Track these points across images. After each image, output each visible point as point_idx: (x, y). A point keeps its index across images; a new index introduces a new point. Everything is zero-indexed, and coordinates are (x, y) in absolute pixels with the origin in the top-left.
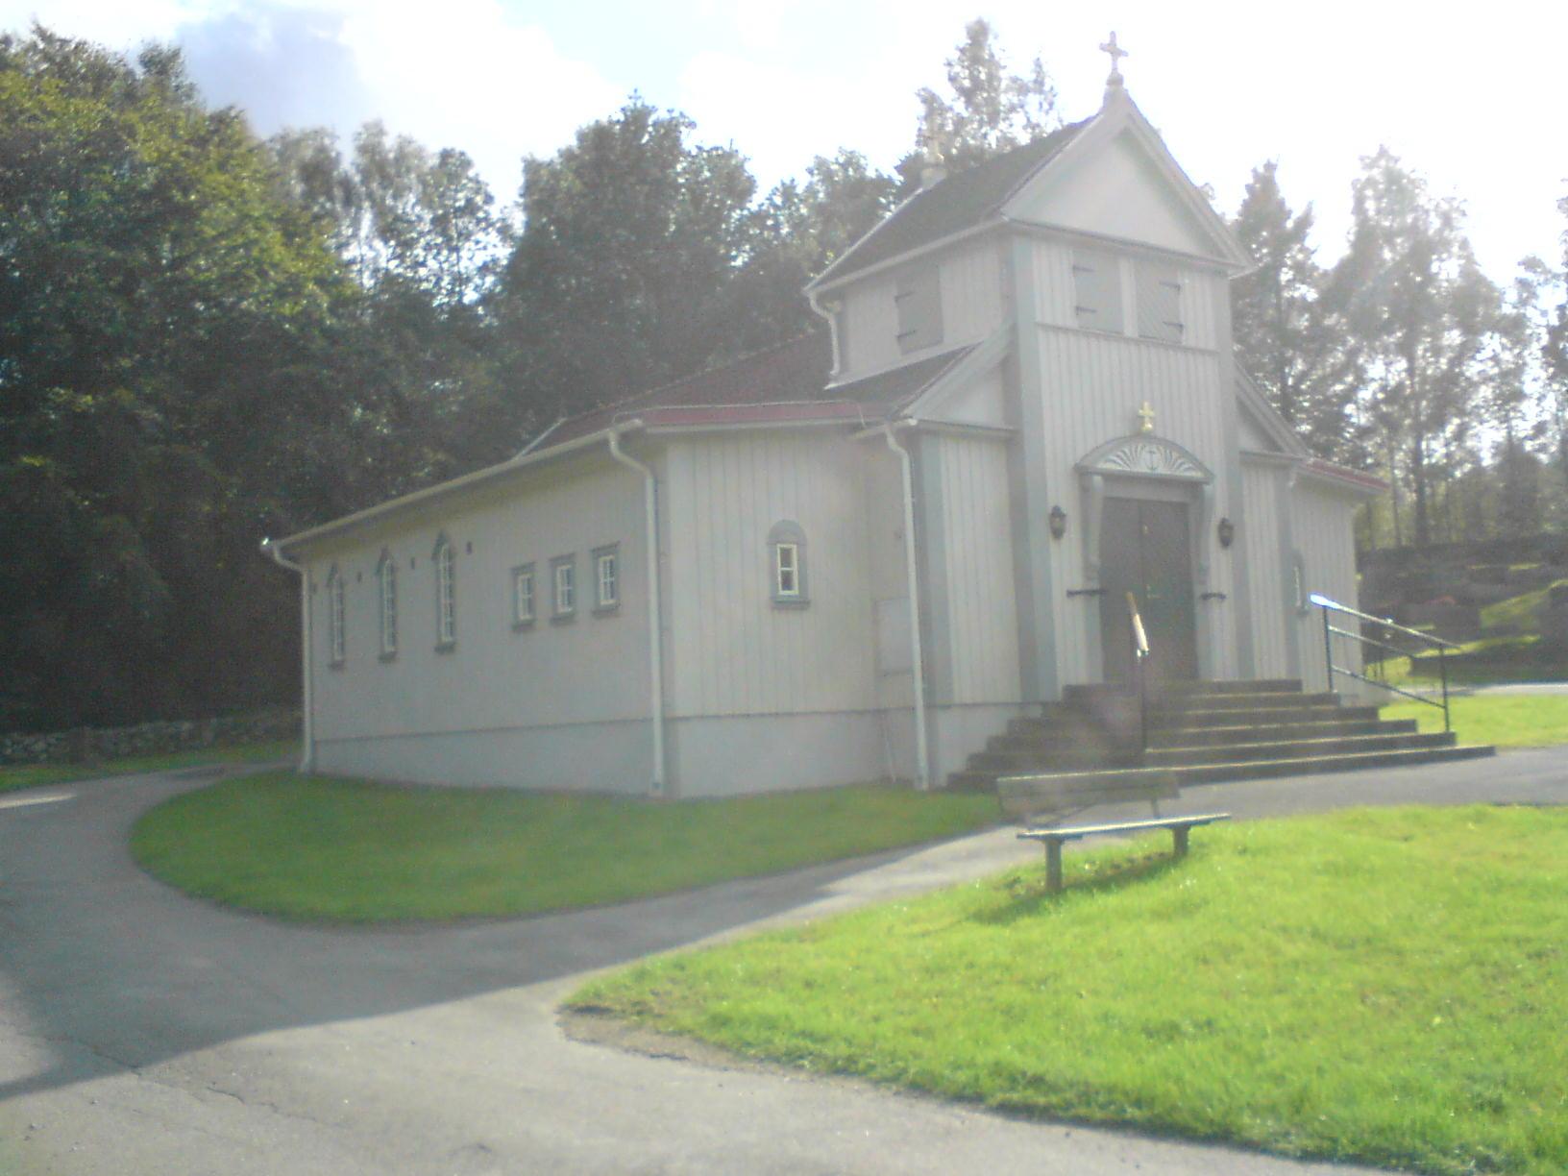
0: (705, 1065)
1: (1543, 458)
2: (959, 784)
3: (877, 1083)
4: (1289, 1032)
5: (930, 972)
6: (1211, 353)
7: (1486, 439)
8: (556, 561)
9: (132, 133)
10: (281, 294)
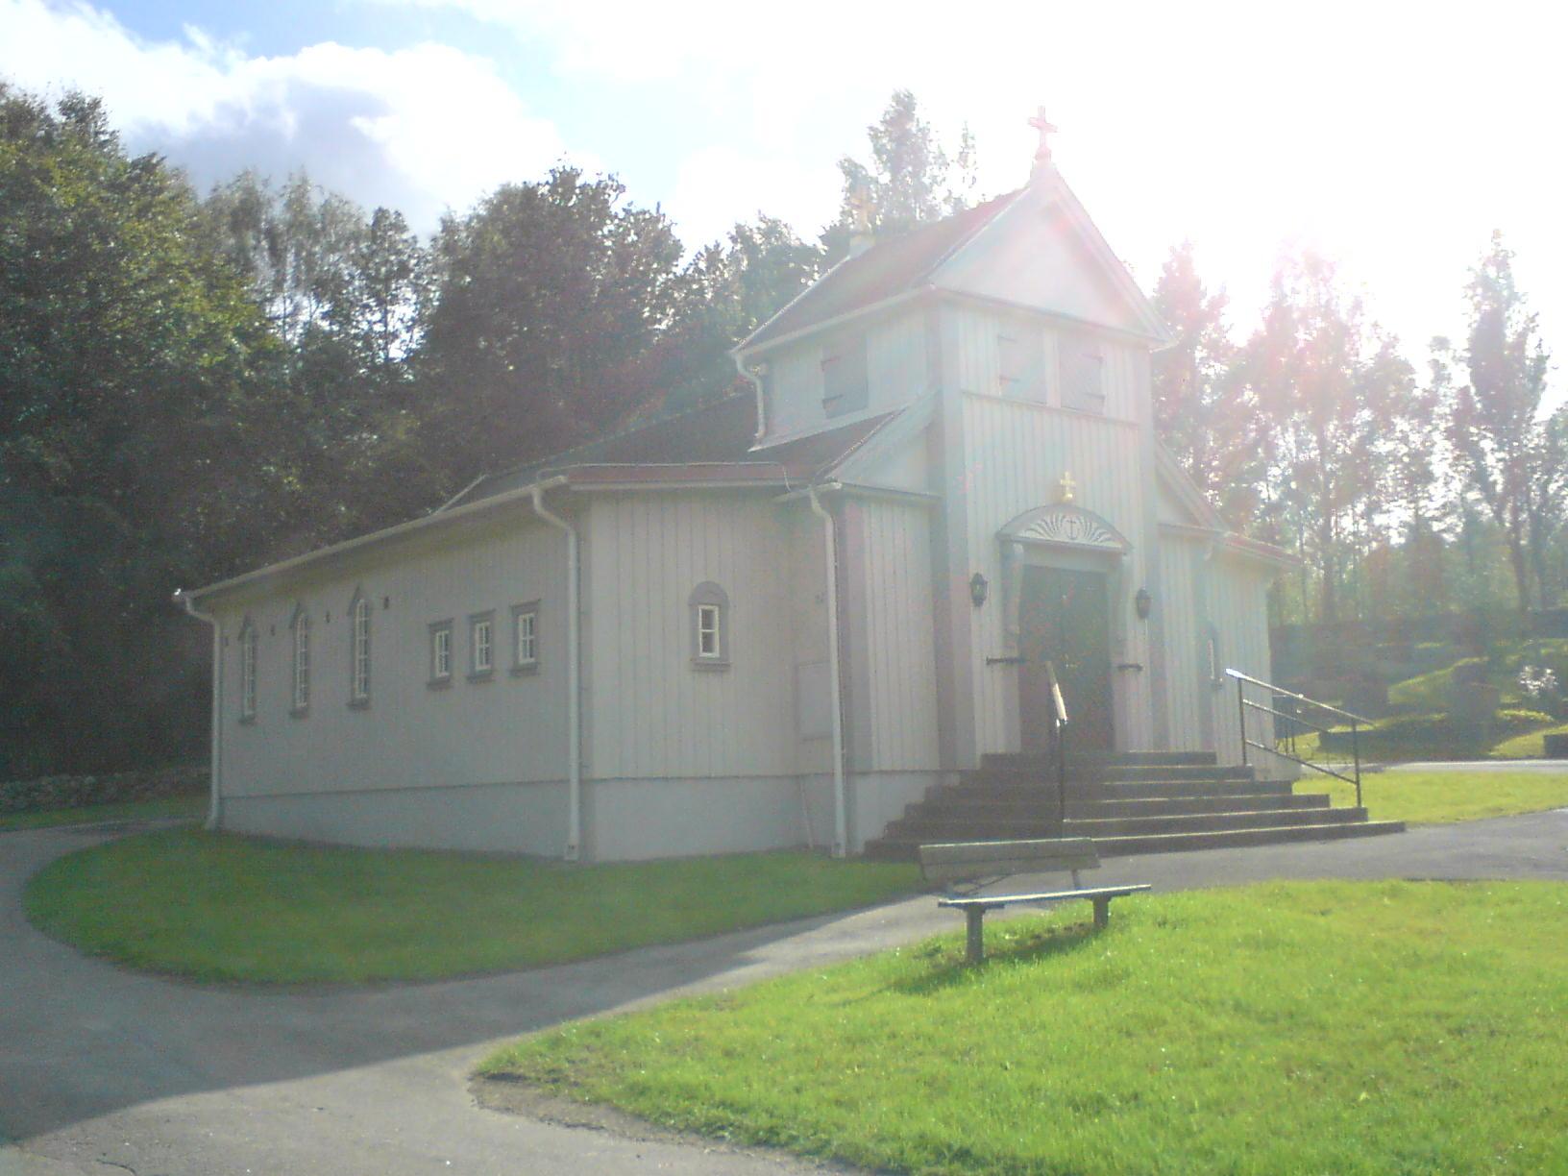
0: (623, 1135)
1: (1449, 537)
2: (876, 851)
3: (798, 1155)
4: (1213, 1106)
5: (852, 1041)
7: (1395, 518)
8: (474, 619)
9: (48, 179)
10: (199, 345)
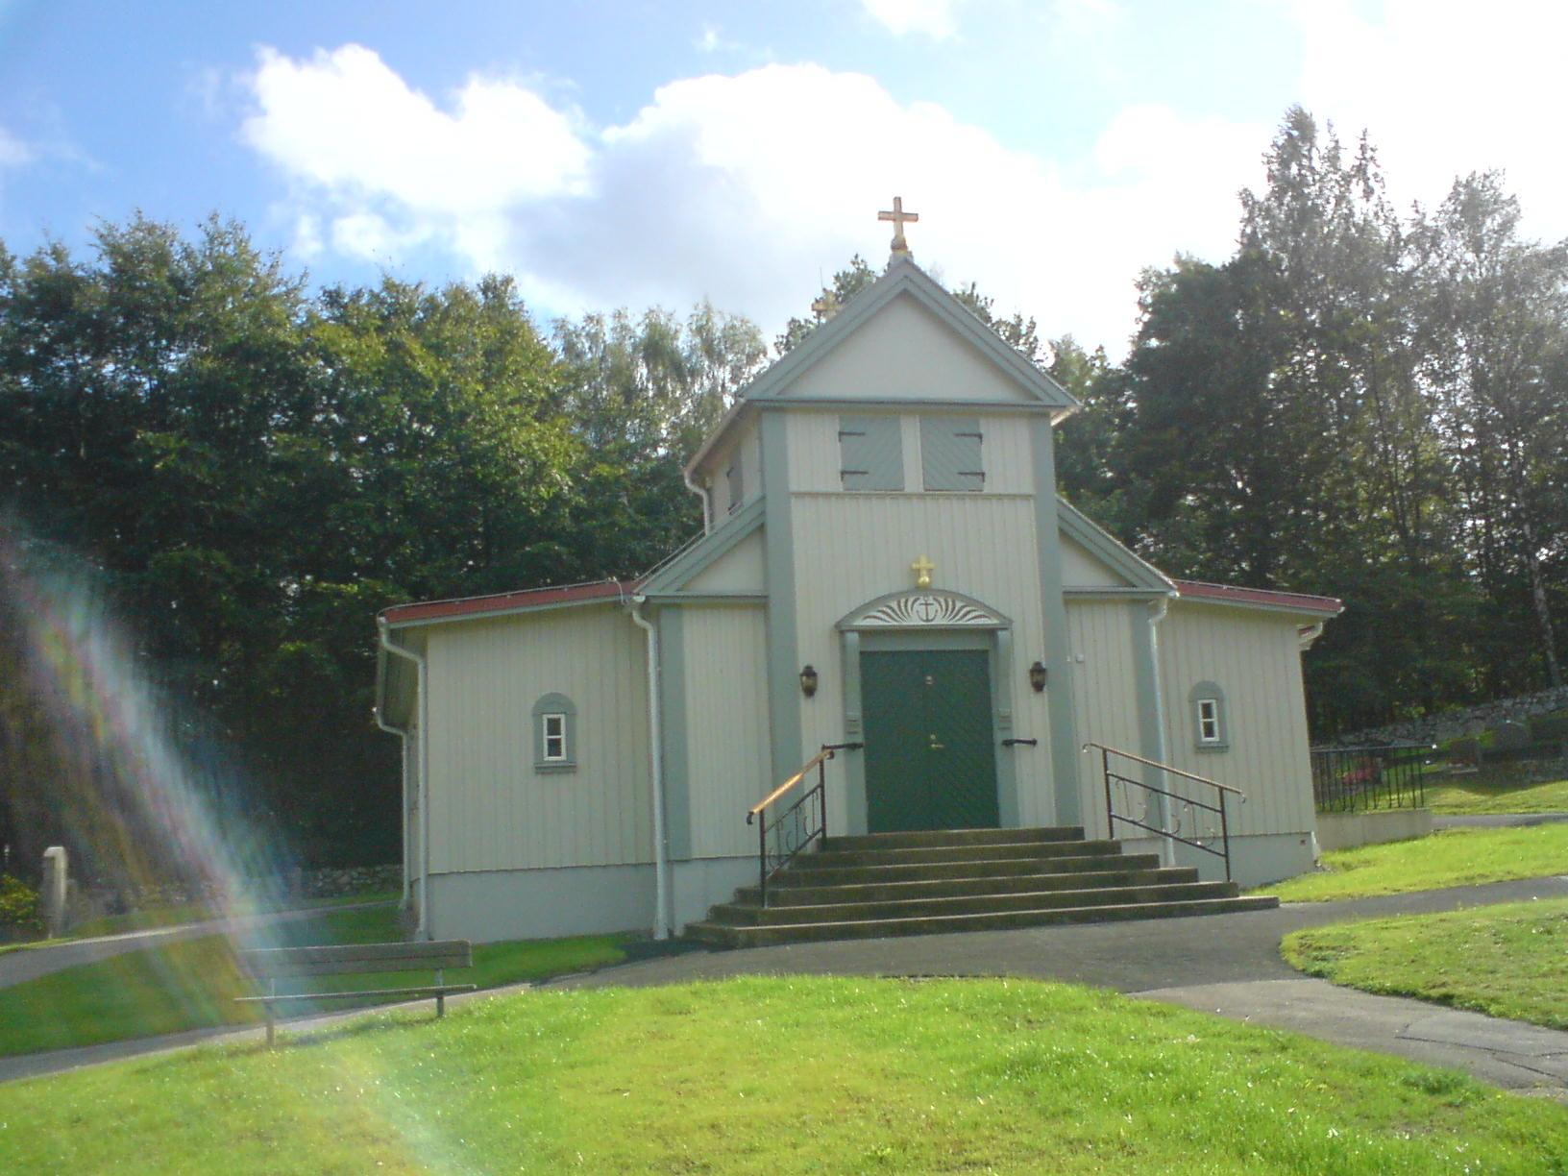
6: (1026, 497)
